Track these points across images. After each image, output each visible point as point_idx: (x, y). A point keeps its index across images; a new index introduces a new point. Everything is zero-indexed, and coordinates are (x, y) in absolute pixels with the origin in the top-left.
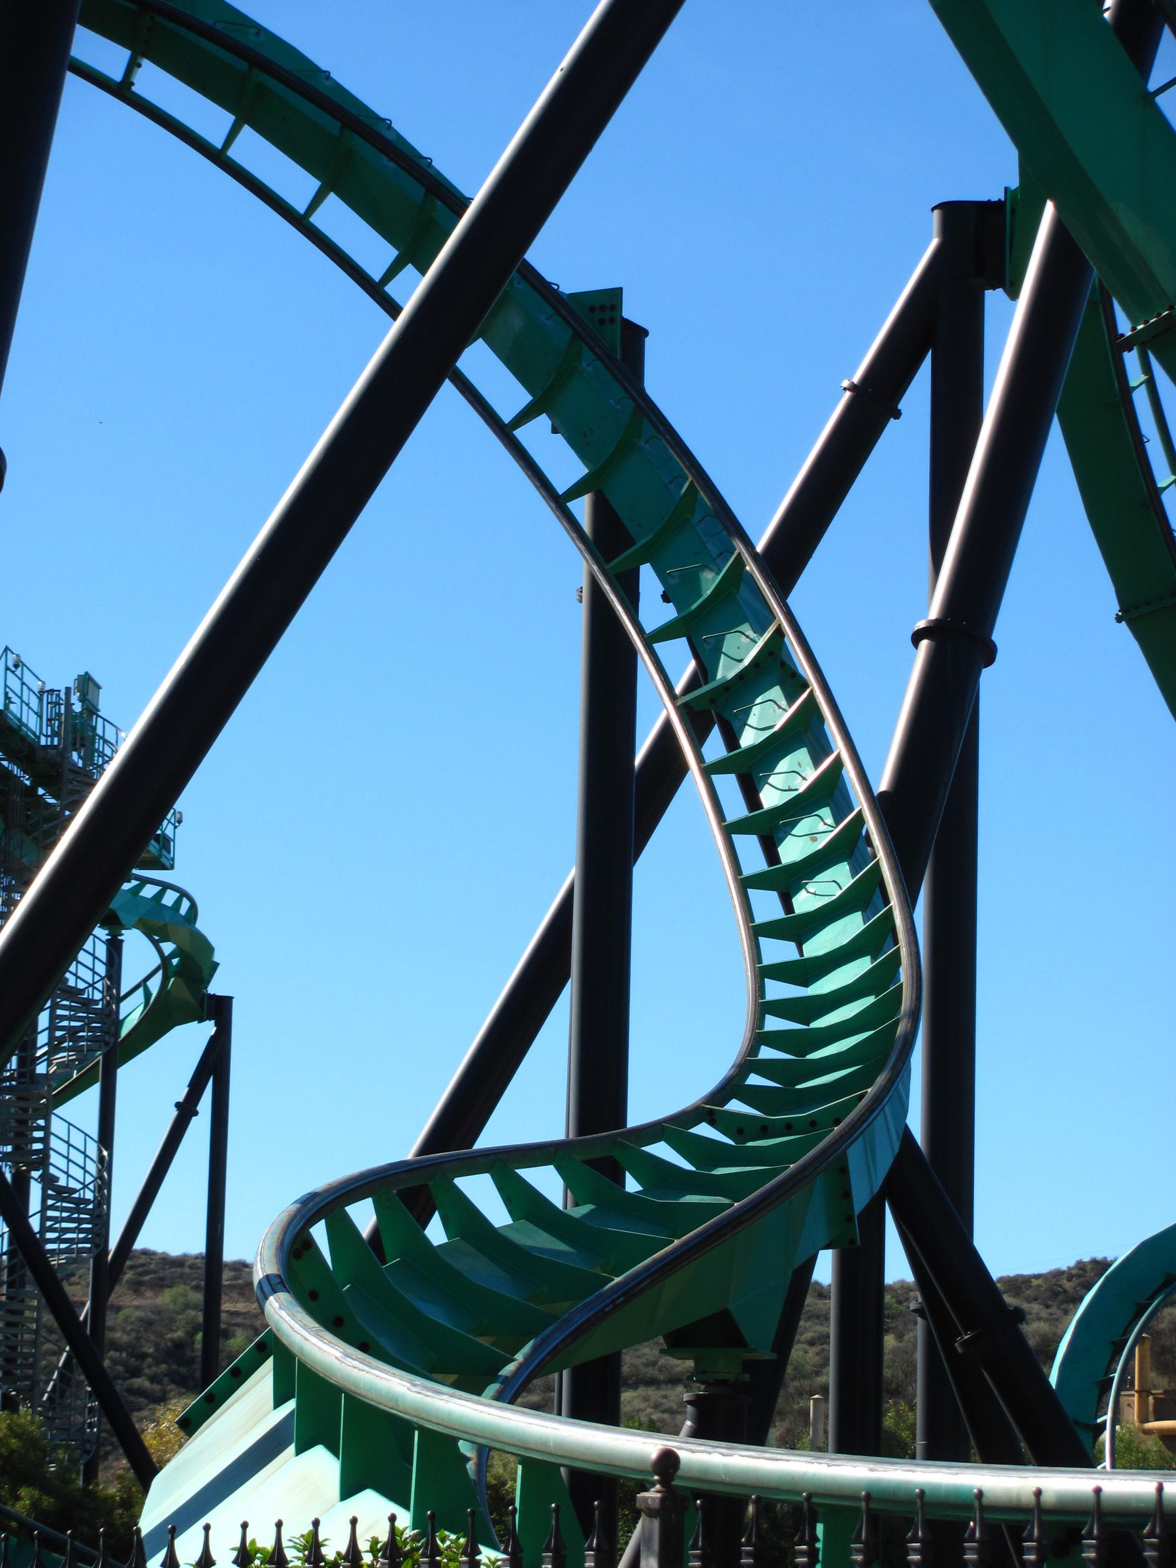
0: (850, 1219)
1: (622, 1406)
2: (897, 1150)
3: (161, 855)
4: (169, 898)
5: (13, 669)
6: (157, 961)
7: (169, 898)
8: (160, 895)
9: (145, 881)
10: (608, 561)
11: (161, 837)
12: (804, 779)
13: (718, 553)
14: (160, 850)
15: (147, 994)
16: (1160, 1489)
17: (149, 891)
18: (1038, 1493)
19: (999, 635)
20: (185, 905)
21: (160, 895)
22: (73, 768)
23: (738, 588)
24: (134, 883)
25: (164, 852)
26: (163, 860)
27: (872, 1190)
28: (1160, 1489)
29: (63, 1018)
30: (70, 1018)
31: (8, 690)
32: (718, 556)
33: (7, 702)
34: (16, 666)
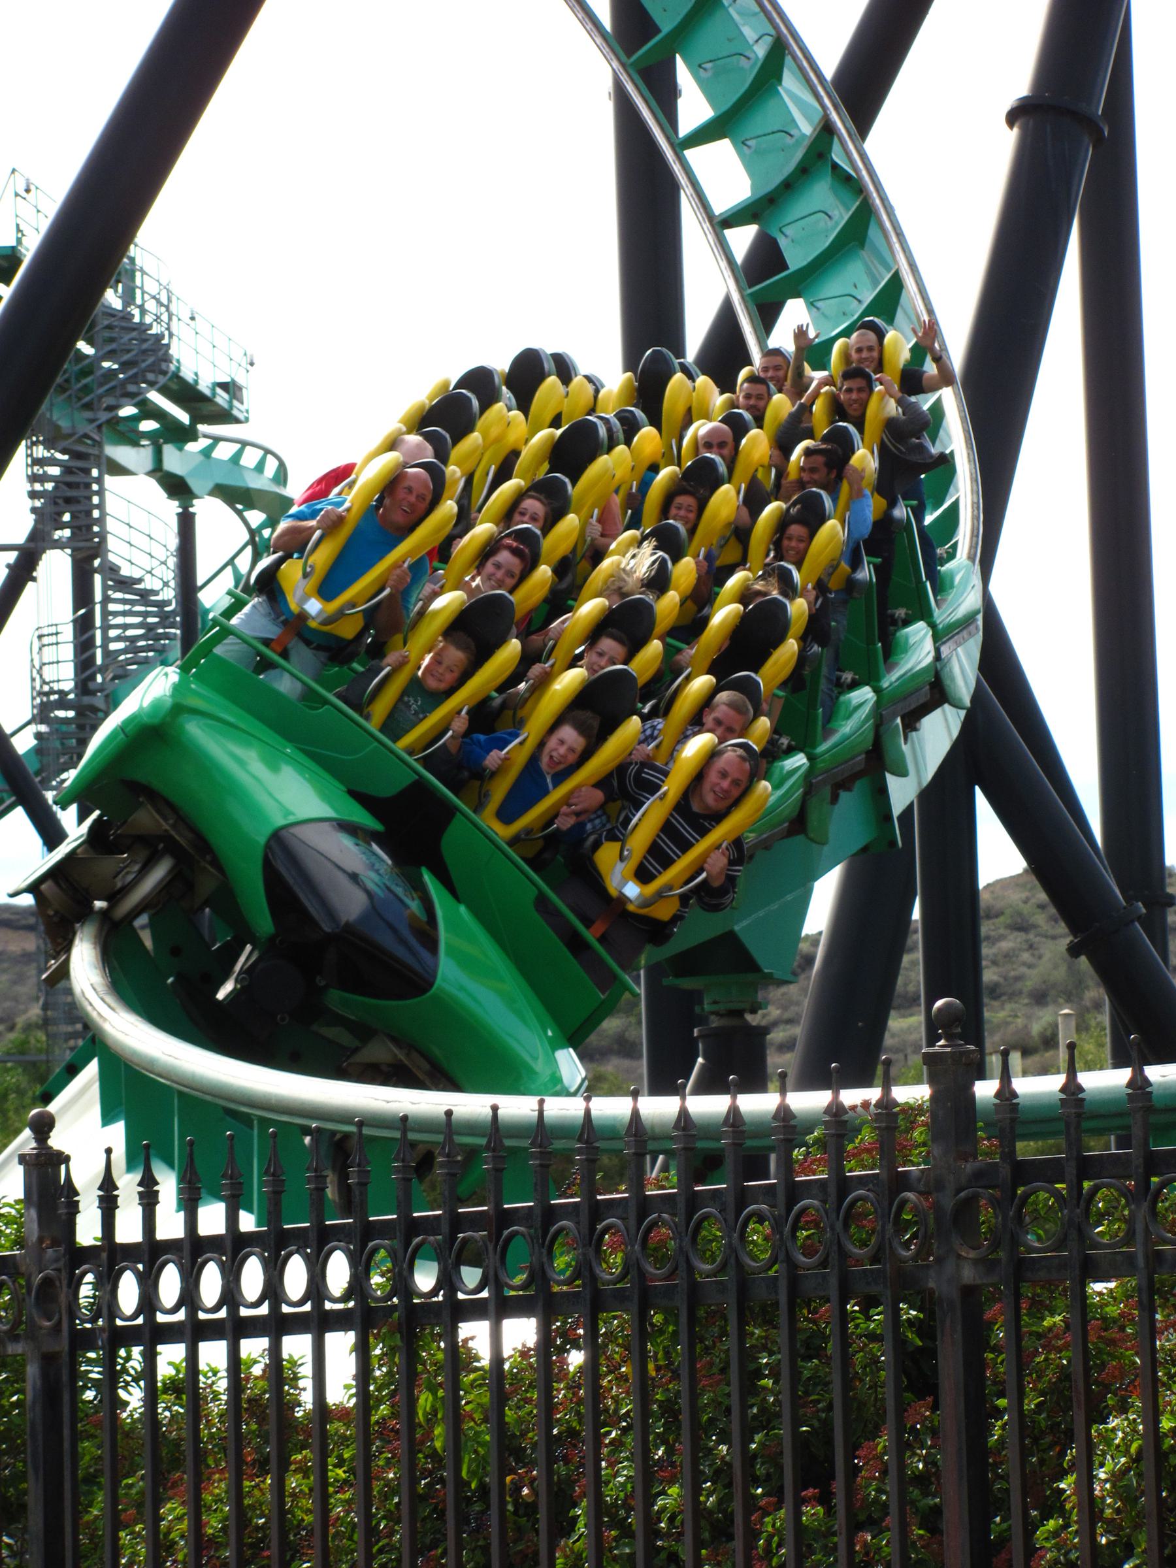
0: (888, 816)
1: (887, 1035)
2: (955, 733)
3: (231, 407)
4: (250, 458)
5: (24, 194)
6: (246, 536)
7: (250, 458)
8: (238, 456)
9: (217, 440)
10: (629, 54)
11: (231, 385)
12: (860, 301)
13: (756, 37)
14: (230, 402)
15: (236, 571)
16: (495, 1109)
17: (224, 452)
18: (449, 1113)
19: (1008, 140)
20: (271, 466)
21: (238, 456)
22: (109, 311)
23: (779, 79)
24: (203, 443)
25: (236, 403)
26: (235, 412)
27: (920, 783)
28: (495, 1109)
29: (116, 614)
30: (124, 614)
31: (19, 221)
32: (757, 41)
33: (20, 235)
34: (28, 191)
